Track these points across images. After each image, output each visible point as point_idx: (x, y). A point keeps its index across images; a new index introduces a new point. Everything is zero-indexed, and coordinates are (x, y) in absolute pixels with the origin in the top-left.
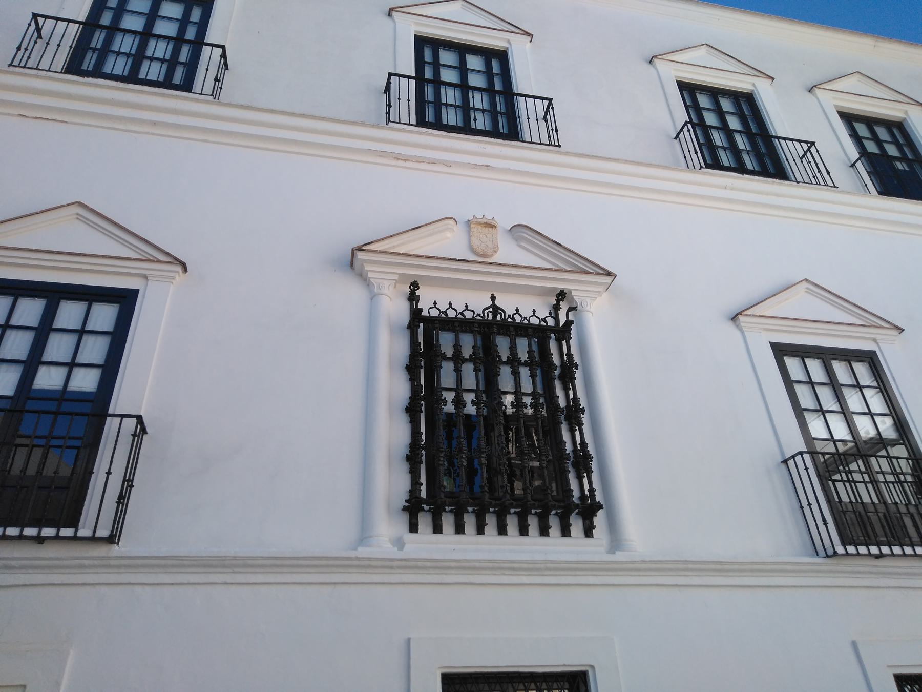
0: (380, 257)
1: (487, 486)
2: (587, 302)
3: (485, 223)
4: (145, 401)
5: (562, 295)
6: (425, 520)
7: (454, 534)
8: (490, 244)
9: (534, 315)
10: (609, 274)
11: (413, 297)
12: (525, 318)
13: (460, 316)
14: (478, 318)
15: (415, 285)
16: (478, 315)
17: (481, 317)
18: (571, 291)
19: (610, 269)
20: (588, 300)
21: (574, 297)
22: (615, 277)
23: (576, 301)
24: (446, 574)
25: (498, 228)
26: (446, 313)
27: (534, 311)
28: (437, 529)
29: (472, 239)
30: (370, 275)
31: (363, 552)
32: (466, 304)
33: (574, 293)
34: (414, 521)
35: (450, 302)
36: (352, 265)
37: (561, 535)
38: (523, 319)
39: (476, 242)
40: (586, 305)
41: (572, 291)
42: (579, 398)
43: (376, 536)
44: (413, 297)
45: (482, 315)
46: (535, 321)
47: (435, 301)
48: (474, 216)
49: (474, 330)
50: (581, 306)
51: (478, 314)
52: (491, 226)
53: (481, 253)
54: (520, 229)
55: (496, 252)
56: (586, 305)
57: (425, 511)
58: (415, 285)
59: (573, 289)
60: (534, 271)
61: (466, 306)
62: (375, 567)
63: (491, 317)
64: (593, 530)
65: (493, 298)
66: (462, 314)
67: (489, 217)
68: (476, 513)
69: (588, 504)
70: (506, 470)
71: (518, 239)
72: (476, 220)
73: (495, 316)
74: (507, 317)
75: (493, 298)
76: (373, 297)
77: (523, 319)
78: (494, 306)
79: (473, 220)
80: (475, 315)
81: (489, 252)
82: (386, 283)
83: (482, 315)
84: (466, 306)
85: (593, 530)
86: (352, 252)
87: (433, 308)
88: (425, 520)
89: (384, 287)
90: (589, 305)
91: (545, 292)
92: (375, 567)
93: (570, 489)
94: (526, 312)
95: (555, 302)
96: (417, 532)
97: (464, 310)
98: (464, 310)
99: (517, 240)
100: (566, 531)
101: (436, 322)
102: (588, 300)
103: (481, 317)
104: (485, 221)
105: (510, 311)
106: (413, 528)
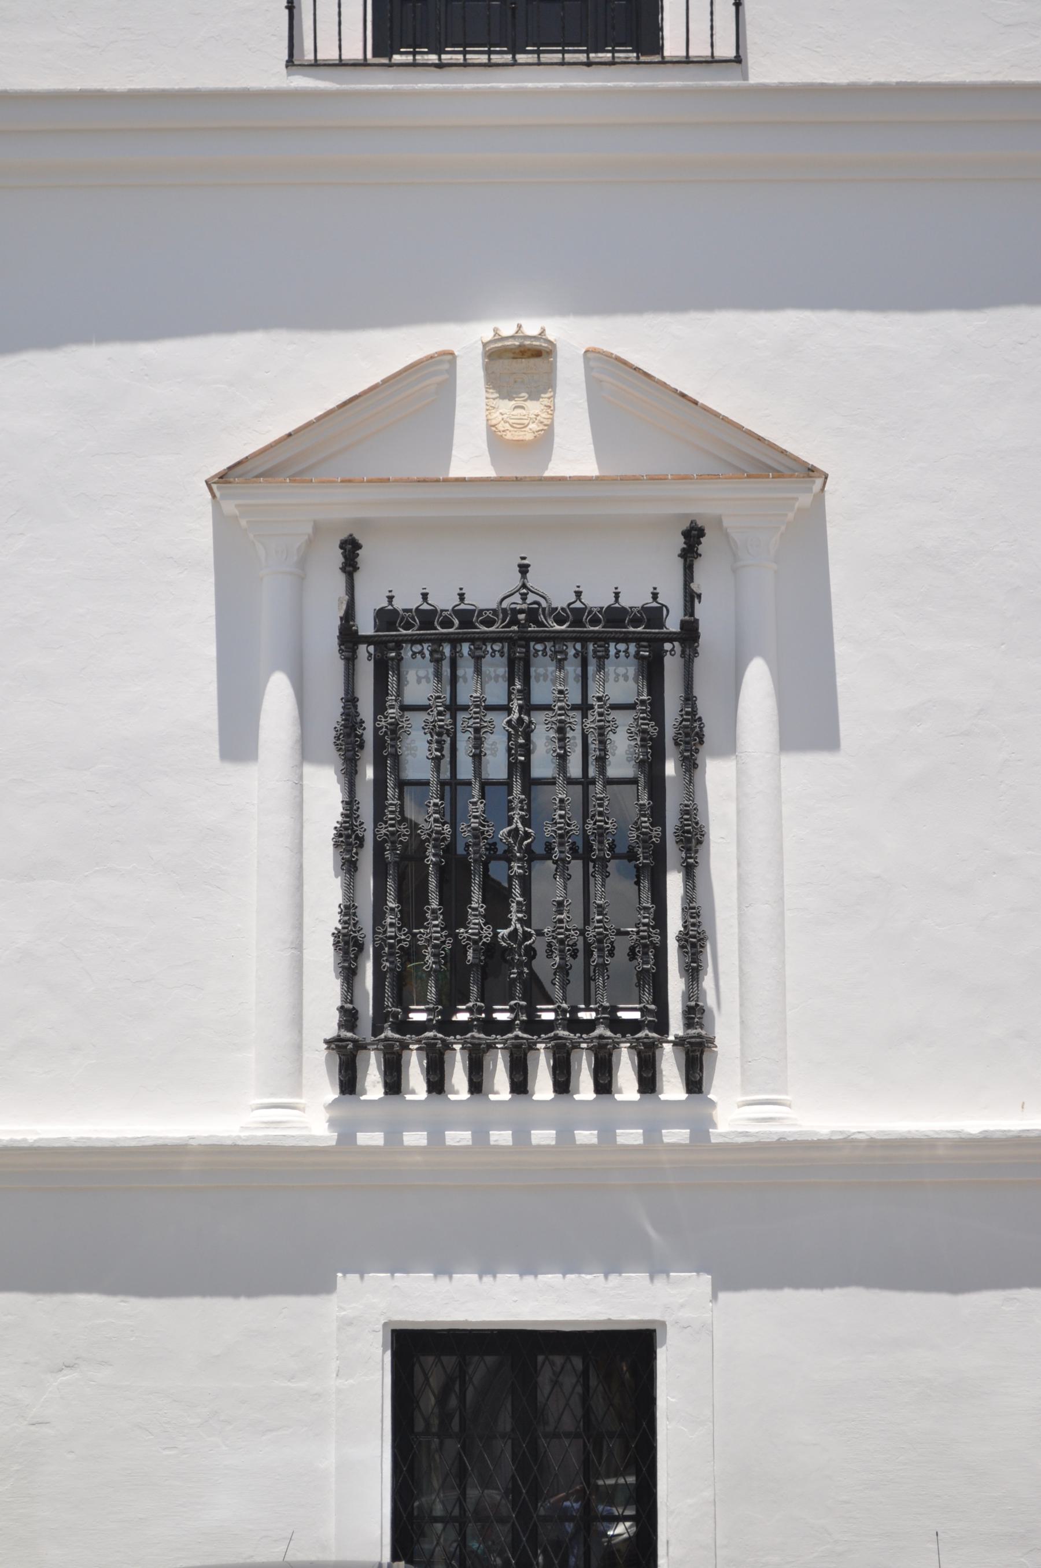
19: (812, 461)
22: (826, 478)
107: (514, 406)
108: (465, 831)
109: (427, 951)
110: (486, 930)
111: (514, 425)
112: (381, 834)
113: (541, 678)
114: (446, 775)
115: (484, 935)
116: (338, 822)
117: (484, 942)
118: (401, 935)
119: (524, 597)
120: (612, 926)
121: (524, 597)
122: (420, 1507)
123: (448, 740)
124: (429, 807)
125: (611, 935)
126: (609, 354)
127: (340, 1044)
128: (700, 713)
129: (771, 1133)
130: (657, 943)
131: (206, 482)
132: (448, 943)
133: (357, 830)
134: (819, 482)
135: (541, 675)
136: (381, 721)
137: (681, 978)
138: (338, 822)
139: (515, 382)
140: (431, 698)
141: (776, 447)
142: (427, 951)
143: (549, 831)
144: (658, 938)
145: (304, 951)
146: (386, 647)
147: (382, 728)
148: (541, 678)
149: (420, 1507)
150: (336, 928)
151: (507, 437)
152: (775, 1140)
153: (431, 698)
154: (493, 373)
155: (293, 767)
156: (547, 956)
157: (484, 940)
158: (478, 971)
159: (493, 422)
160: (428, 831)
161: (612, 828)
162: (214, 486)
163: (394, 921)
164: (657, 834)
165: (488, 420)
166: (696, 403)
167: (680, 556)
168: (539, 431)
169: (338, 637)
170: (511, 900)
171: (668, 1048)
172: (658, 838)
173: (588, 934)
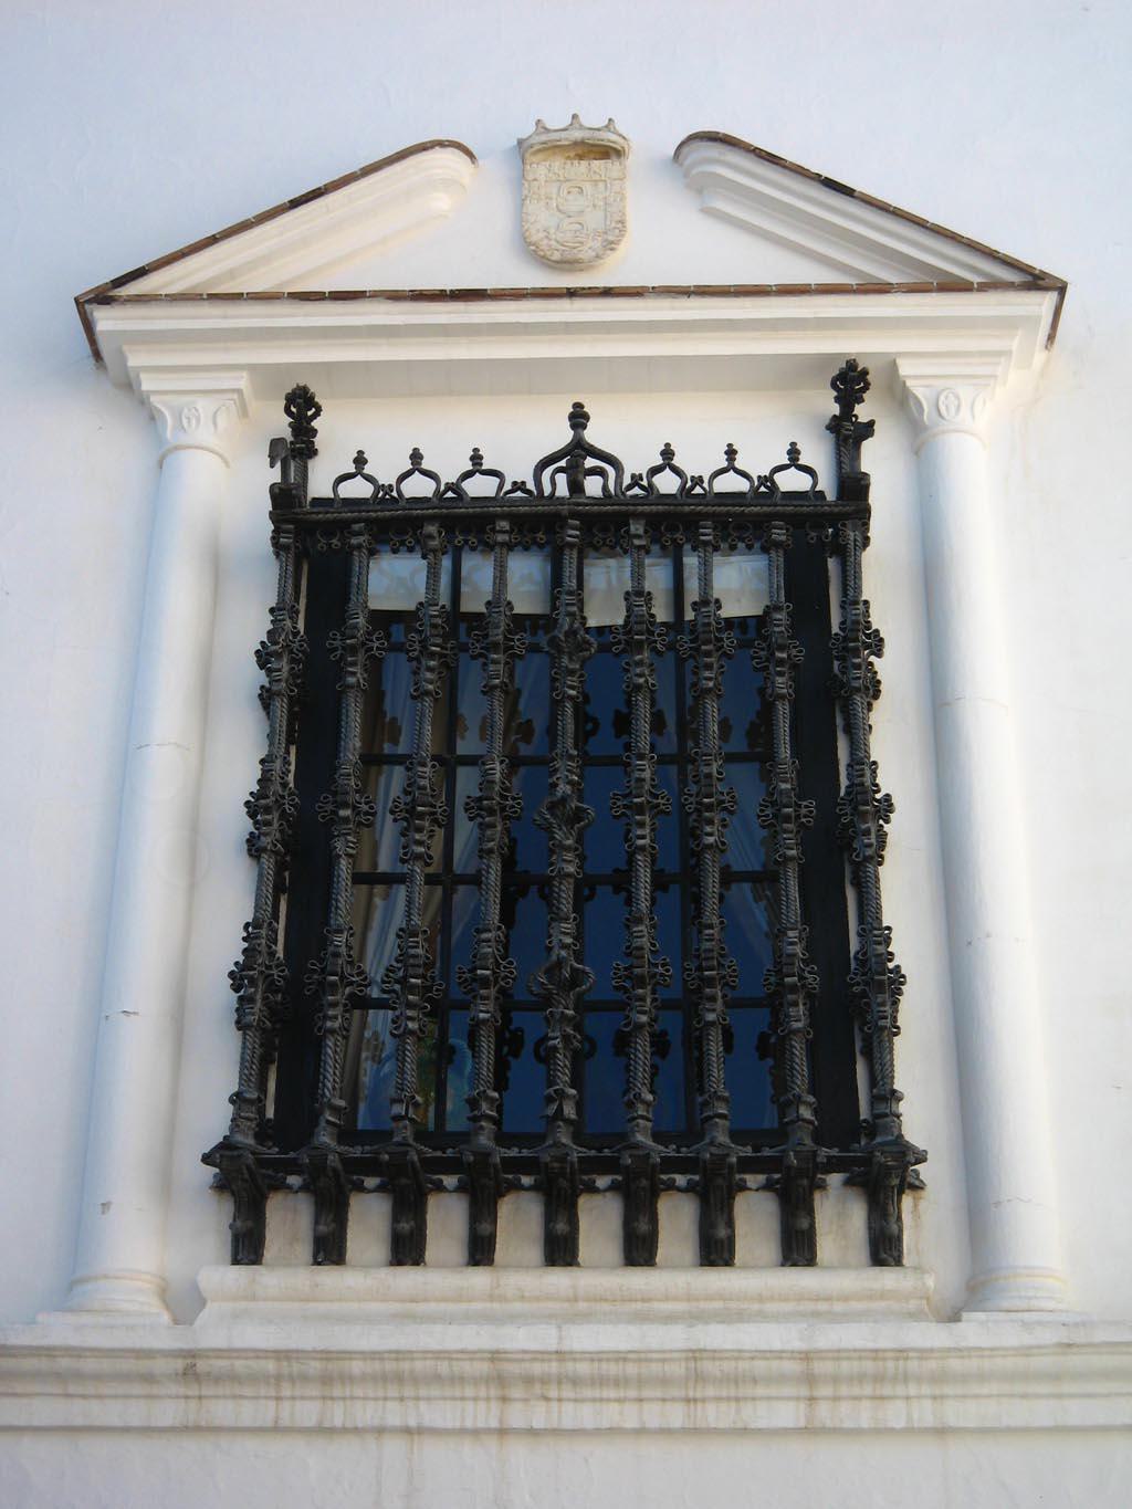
0: (530, 311)
1: (809, 1104)
2: (957, 397)
3: (576, 144)
5: (850, 382)
6: (289, 1219)
7: (695, 1266)
8: (594, 220)
9: (731, 467)
10: (1036, 281)
11: (297, 448)
12: (698, 481)
15: (302, 405)
18: (894, 362)
19: (1040, 263)
20: (965, 392)
21: (908, 383)
23: (916, 398)
24: (100, 1397)
25: (631, 160)
26: (773, 483)
27: (731, 453)
28: (560, 1250)
29: (531, 207)
30: (147, 384)
31: (59, 1330)
33: (905, 368)
34: (484, 1228)
35: (476, 450)
36: (97, 355)
37: (697, 1259)
38: (689, 484)
40: (953, 410)
41: (899, 361)
43: (106, 1277)
44: (297, 448)
47: (476, 450)
48: (575, 117)
49: (496, 543)
50: (935, 414)
51: (515, 483)
52: (600, 150)
53: (556, 256)
54: (714, 150)
55: (611, 246)
56: (953, 410)
57: (750, 1189)
58: (302, 405)
59: (900, 354)
60: (695, 302)
61: (476, 458)
62: (98, 1377)
63: (563, 490)
65: (579, 418)
67: (593, 119)
68: (775, 1191)
70: (566, 1038)
71: (699, 187)
72: (544, 138)
73: (576, 487)
75: (579, 418)
76: (163, 458)
77: (689, 484)
79: (532, 141)
81: (585, 254)
82: (204, 406)
83: (531, 486)
84: (476, 458)
88: (289, 1219)
89: (198, 420)
90: (965, 410)
91: (786, 374)
92: (98, 1377)
93: (894, 1092)
94: (699, 460)
95: (836, 409)
96: (418, 1260)
97: (467, 475)
98: (467, 475)
99: (700, 191)
100: (798, 1247)
101: (356, 527)
102: (965, 392)
103: (529, 492)
104: (577, 135)
105: (638, 460)
106: (247, 1247)
110: (505, 967)
115: (502, 974)
122: (559, 1127)
125: (730, 976)
127: (228, 1153)
128: (870, 611)
130: (815, 988)
132: (437, 990)
136: (334, 640)
137: (863, 401)
139: (569, 193)
147: (336, 649)
149: (559, 1127)
154: (535, 180)
155: (147, 745)
158: (489, 1036)
163: (420, 769)
165: (525, 238)
167: (828, 428)
169: (270, 512)
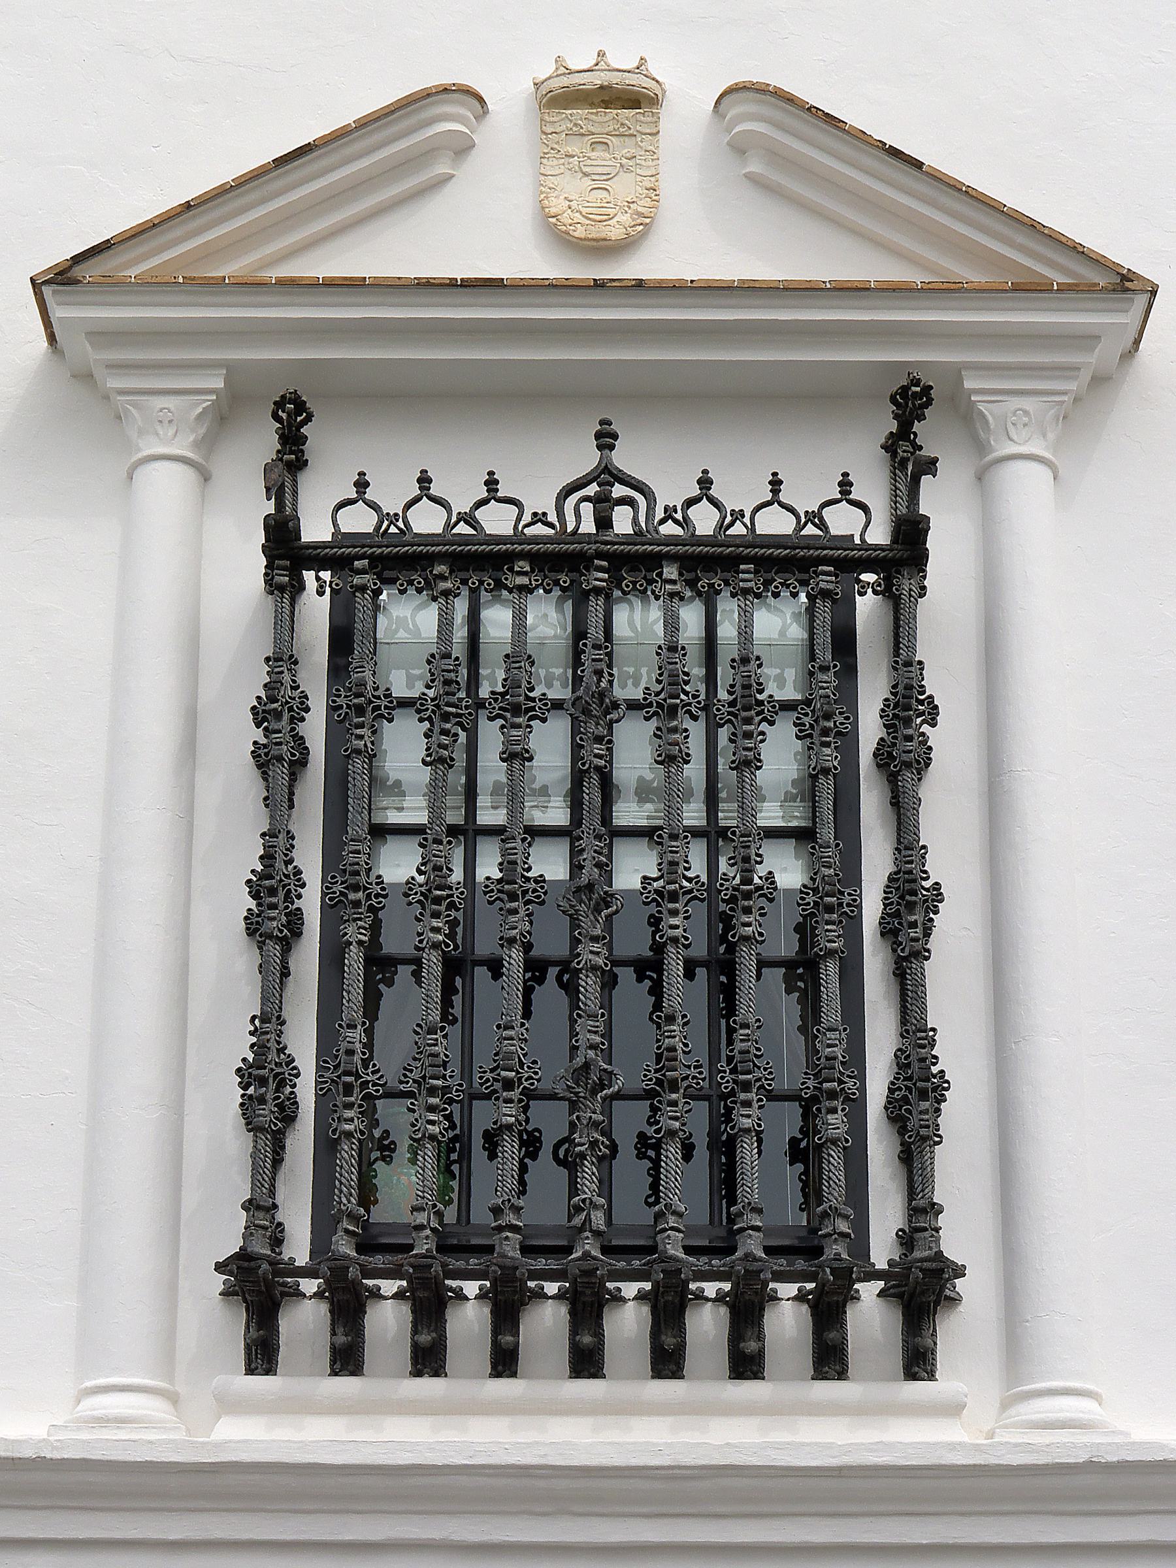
4: (1025, 1388)
9: (775, 500)
12: (738, 515)
13: (463, 529)
14: (539, 529)
16: (539, 518)
17: (551, 526)
19: (1127, 261)
22: (1154, 293)
32: (491, 473)
35: (424, 472)
38: (729, 519)
39: (556, 204)
42: (934, 1030)
45: (552, 517)
46: (776, 523)
51: (535, 514)
64: (296, 1264)
66: (468, 518)
67: (622, 58)
69: (654, 787)
74: (660, 514)
77: (729, 519)
78: (607, 474)
80: (527, 518)
83: (552, 517)
85: (296, 1264)
86: (35, 294)
87: (350, 502)
103: (551, 526)
107: (590, 188)
108: (492, 891)
109: (416, 1103)
110: (529, 1067)
111: (590, 216)
112: (335, 893)
113: (630, 682)
114: (455, 817)
116: (253, 871)
117: (525, 1088)
118: (368, 1074)
119: (604, 506)
120: (768, 1063)
121: (604, 506)
123: (463, 737)
124: (423, 949)
125: (767, 1079)
126: (763, 86)
127: (246, 1264)
129: (1074, 1446)
131: (31, 278)
133: (290, 884)
134: (1141, 300)
135: (629, 678)
136: (339, 696)
138: (253, 871)
140: (418, 1029)
141: (1064, 240)
142: (416, 1103)
143: (650, 892)
144: (856, 1083)
145: (186, 1118)
146: (352, 570)
148: (630, 682)
150: (244, 1060)
151: (576, 234)
152: (1081, 1461)
153: (418, 1029)
156: (638, 1157)
157: (526, 1084)
159: (553, 211)
160: (423, 889)
161: (768, 888)
162: (47, 291)
164: (852, 900)
165: (543, 208)
166: (918, 165)
168: (634, 226)
170: (577, 1014)
171: (869, 1291)
172: (854, 906)
173: (722, 1078)
